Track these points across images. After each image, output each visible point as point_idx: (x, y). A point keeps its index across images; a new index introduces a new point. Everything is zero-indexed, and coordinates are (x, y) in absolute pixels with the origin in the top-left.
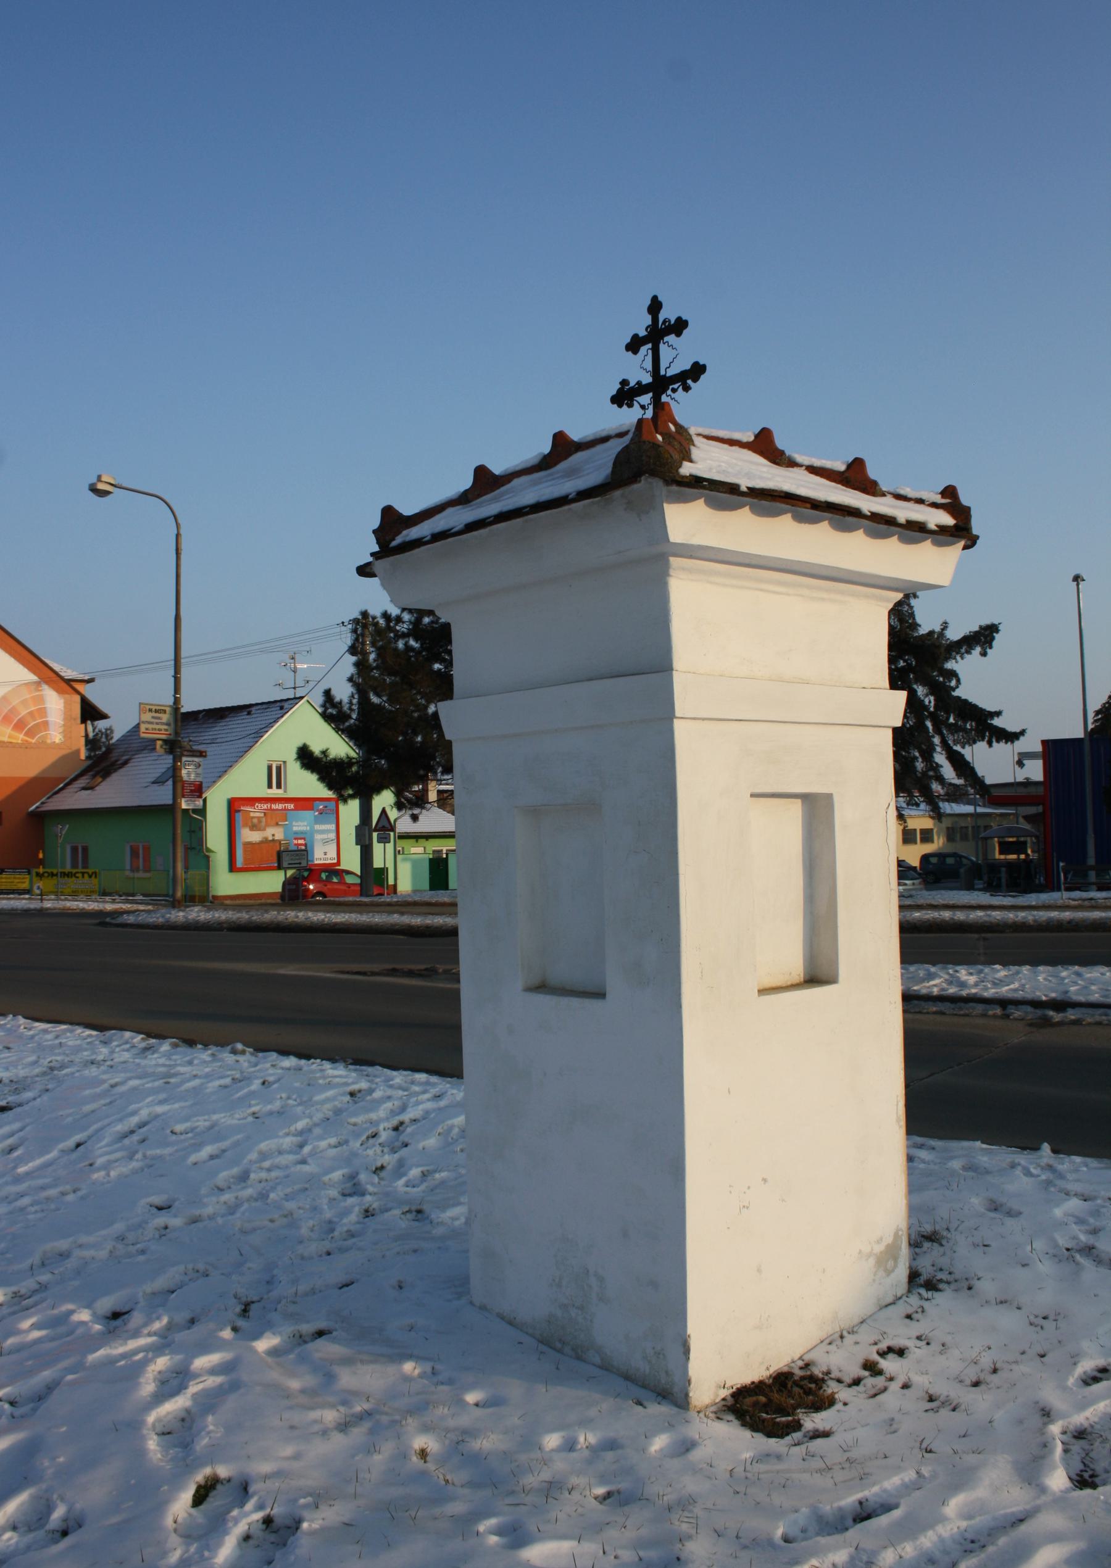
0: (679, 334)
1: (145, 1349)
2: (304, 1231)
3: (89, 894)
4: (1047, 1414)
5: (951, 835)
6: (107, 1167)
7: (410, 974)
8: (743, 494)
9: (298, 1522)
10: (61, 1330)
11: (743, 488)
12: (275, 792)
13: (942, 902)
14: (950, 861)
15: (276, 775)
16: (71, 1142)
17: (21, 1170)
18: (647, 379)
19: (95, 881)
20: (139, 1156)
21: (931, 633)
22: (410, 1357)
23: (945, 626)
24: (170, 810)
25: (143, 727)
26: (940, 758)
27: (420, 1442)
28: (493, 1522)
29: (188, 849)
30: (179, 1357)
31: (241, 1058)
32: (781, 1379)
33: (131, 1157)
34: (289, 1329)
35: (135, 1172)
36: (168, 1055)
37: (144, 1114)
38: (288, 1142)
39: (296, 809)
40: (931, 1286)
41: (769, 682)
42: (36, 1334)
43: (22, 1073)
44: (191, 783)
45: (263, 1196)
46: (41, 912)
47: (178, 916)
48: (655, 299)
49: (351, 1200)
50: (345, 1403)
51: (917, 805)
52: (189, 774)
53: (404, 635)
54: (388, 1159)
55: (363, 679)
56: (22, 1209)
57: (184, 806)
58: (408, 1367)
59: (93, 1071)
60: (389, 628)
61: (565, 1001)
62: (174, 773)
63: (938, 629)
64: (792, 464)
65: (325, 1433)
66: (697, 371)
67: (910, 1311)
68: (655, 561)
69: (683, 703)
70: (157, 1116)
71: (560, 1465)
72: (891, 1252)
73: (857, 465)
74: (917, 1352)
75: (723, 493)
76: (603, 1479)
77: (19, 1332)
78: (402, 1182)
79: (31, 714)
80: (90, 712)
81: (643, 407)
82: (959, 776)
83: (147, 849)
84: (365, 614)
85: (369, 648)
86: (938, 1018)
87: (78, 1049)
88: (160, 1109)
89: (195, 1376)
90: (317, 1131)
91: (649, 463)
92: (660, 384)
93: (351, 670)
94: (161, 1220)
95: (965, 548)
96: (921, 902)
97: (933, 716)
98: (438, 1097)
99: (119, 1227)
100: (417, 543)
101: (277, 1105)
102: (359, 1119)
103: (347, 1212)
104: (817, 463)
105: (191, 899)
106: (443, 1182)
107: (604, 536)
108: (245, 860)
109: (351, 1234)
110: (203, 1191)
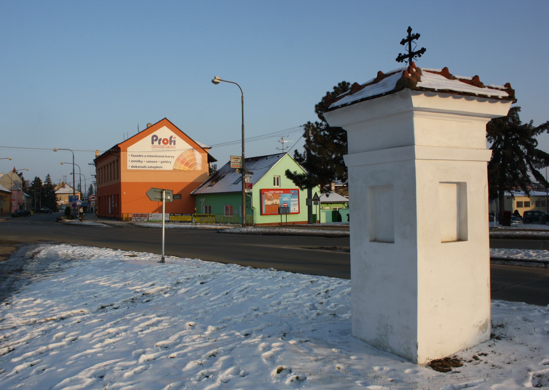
0: (417, 39)
1: (259, 341)
2: (299, 318)
3: (212, 223)
4: (529, 370)
5: (537, 204)
6: (237, 299)
7: (327, 249)
8: (436, 92)
9: (306, 378)
10: (233, 336)
11: (436, 90)
12: (276, 187)
13: (529, 228)
14: (536, 214)
15: (276, 181)
16: (225, 292)
17: (211, 299)
18: (407, 53)
19: (214, 218)
20: (246, 296)
21: (526, 125)
22: (334, 348)
23: (532, 122)
24: (241, 193)
25: (232, 164)
26: (529, 173)
27: (338, 365)
28: (359, 381)
29: (247, 207)
30: (268, 343)
31: (273, 272)
32: (447, 359)
33: (244, 297)
34: (298, 339)
35: (245, 301)
36: (248, 271)
37: (246, 285)
38: (292, 294)
39: (284, 193)
40: (498, 338)
41: (449, 147)
42: (226, 337)
43: (205, 274)
44: (248, 184)
45: (286, 308)
46: (196, 229)
47: (245, 230)
48: (409, 27)
49: (312, 311)
50: (316, 356)
51: (519, 191)
52: (247, 180)
53: (323, 130)
54: (324, 300)
55: (309, 146)
56: (215, 308)
57: (246, 192)
58: (334, 350)
59: (228, 274)
60: (318, 128)
61: (382, 244)
62: (242, 179)
63: (529, 123)
64: (454, 78)
65: (311, 361)
66: (423, 50)
67: (490, 344)
68: (410, 112)
69: (418, 154)
70: (250, 286)
71: (379, 373)
72: (484, 326)
73: (476, 78)
74: (491, 355)
75: (429, 92)
76: (390, 377)
77: (221, 336)
78: (328, 307)
79: (190, 160)
80: (211, 159)
81: (406, 62)
82: (537, 180)
83: (231, 207)
84: (309, 123)
85: (311, 135)
86: (519, 267)
87: (221, 268)
88: (251, 284)
89: (273, 347)
90: (301, 292)
91: (407, 83)
92: (411, 55)
93: (305, 143)
94: (256, 313)
95: (513, 103)
96: (520, 228)
97: (527, 157)
98: (339, 283)
99: (244, 314)
100: (337, 107)
101: (288, 284)
102: (314, 289)
103: (312, 314)
104: (463, 78)
105: (247, 225)
106: (341, 308)
107: (393, 105)
108: (266, 211)
109: (313, 319)
110: (268, 306)
